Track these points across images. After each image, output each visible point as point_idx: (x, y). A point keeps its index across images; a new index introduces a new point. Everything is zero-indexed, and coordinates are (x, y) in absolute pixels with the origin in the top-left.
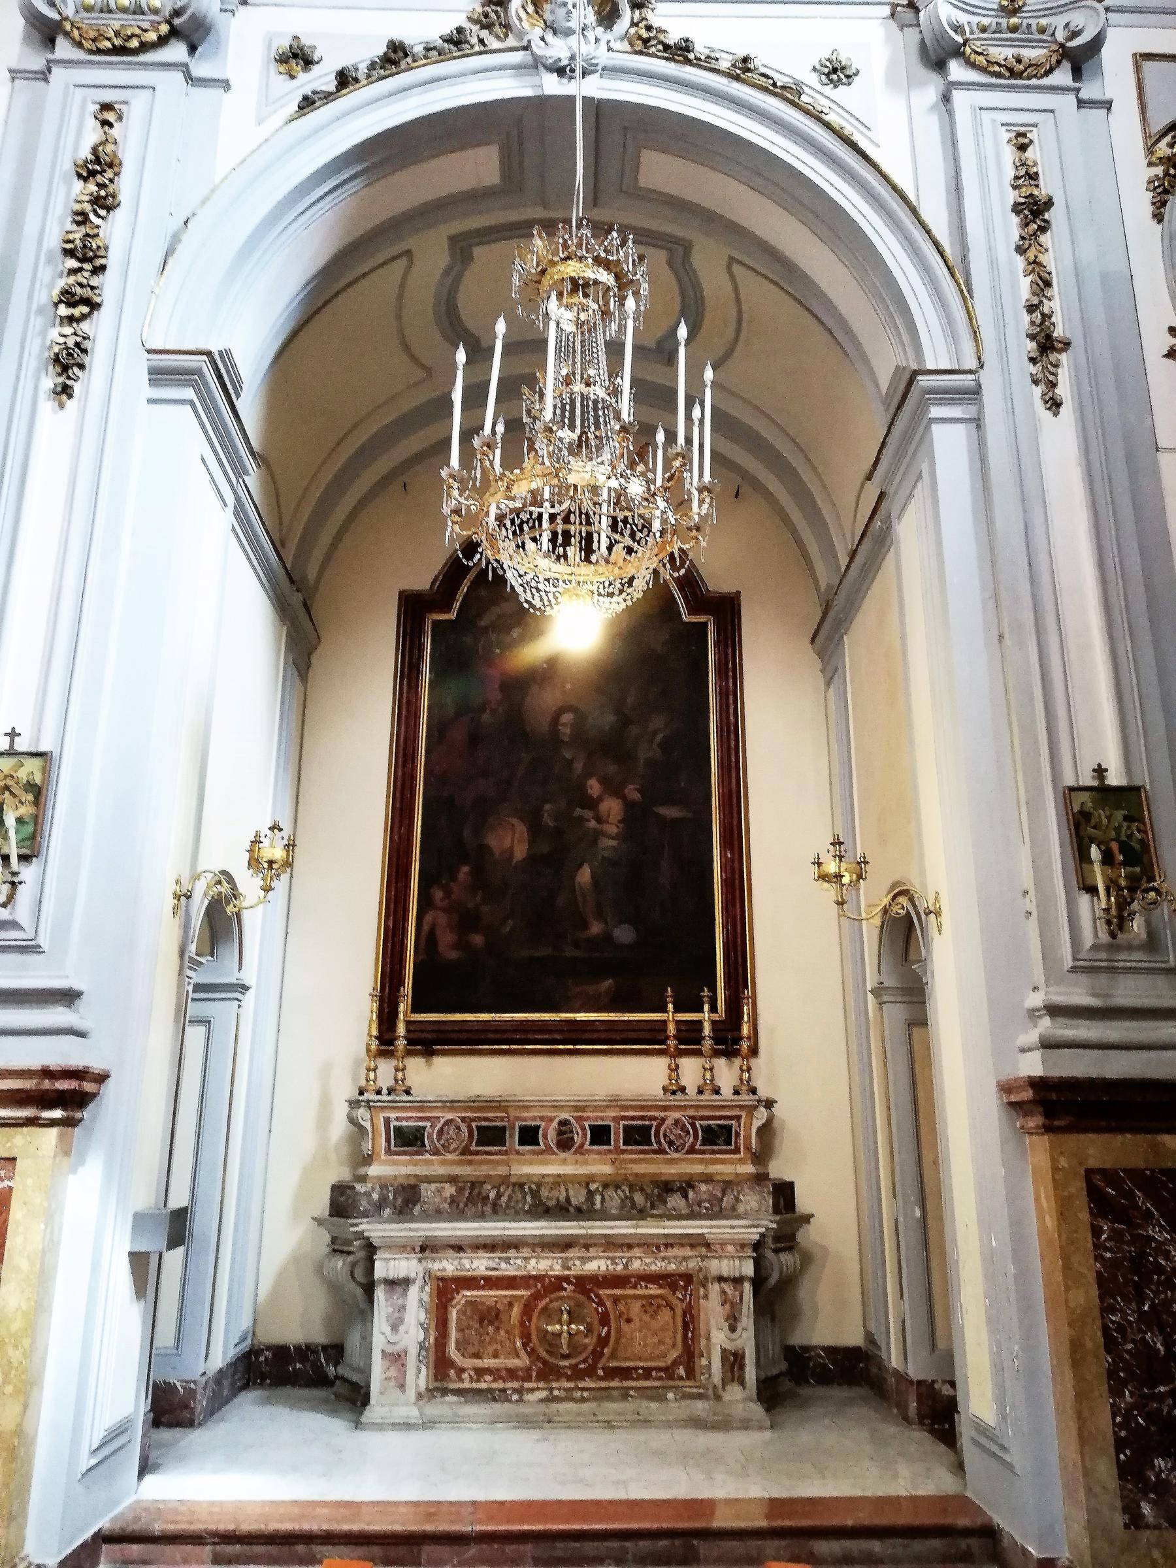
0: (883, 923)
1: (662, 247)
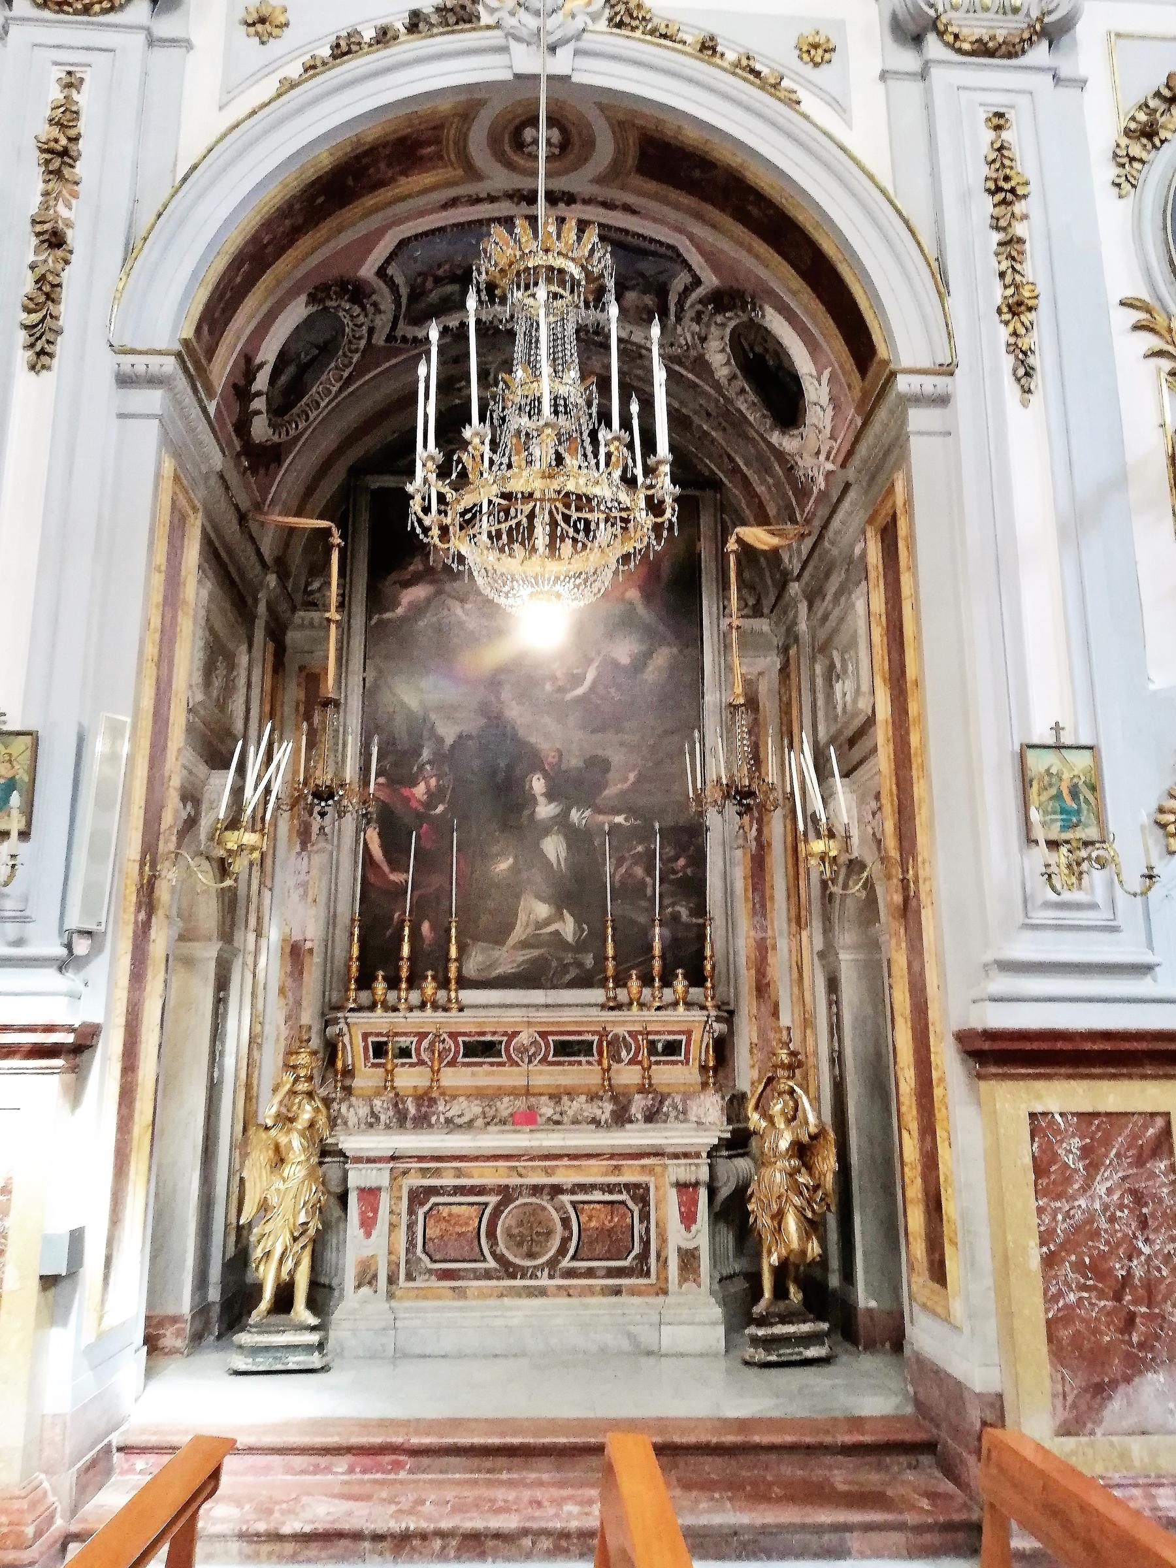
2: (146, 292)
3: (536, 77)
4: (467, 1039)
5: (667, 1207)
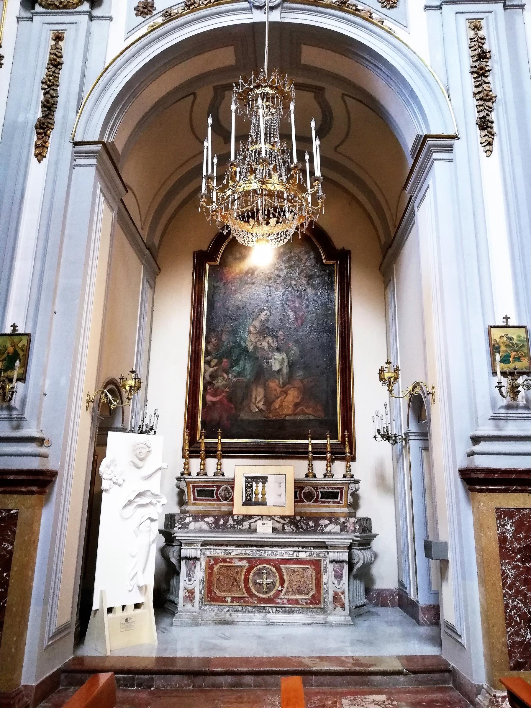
0: (410, 398)
1: (311, 91)
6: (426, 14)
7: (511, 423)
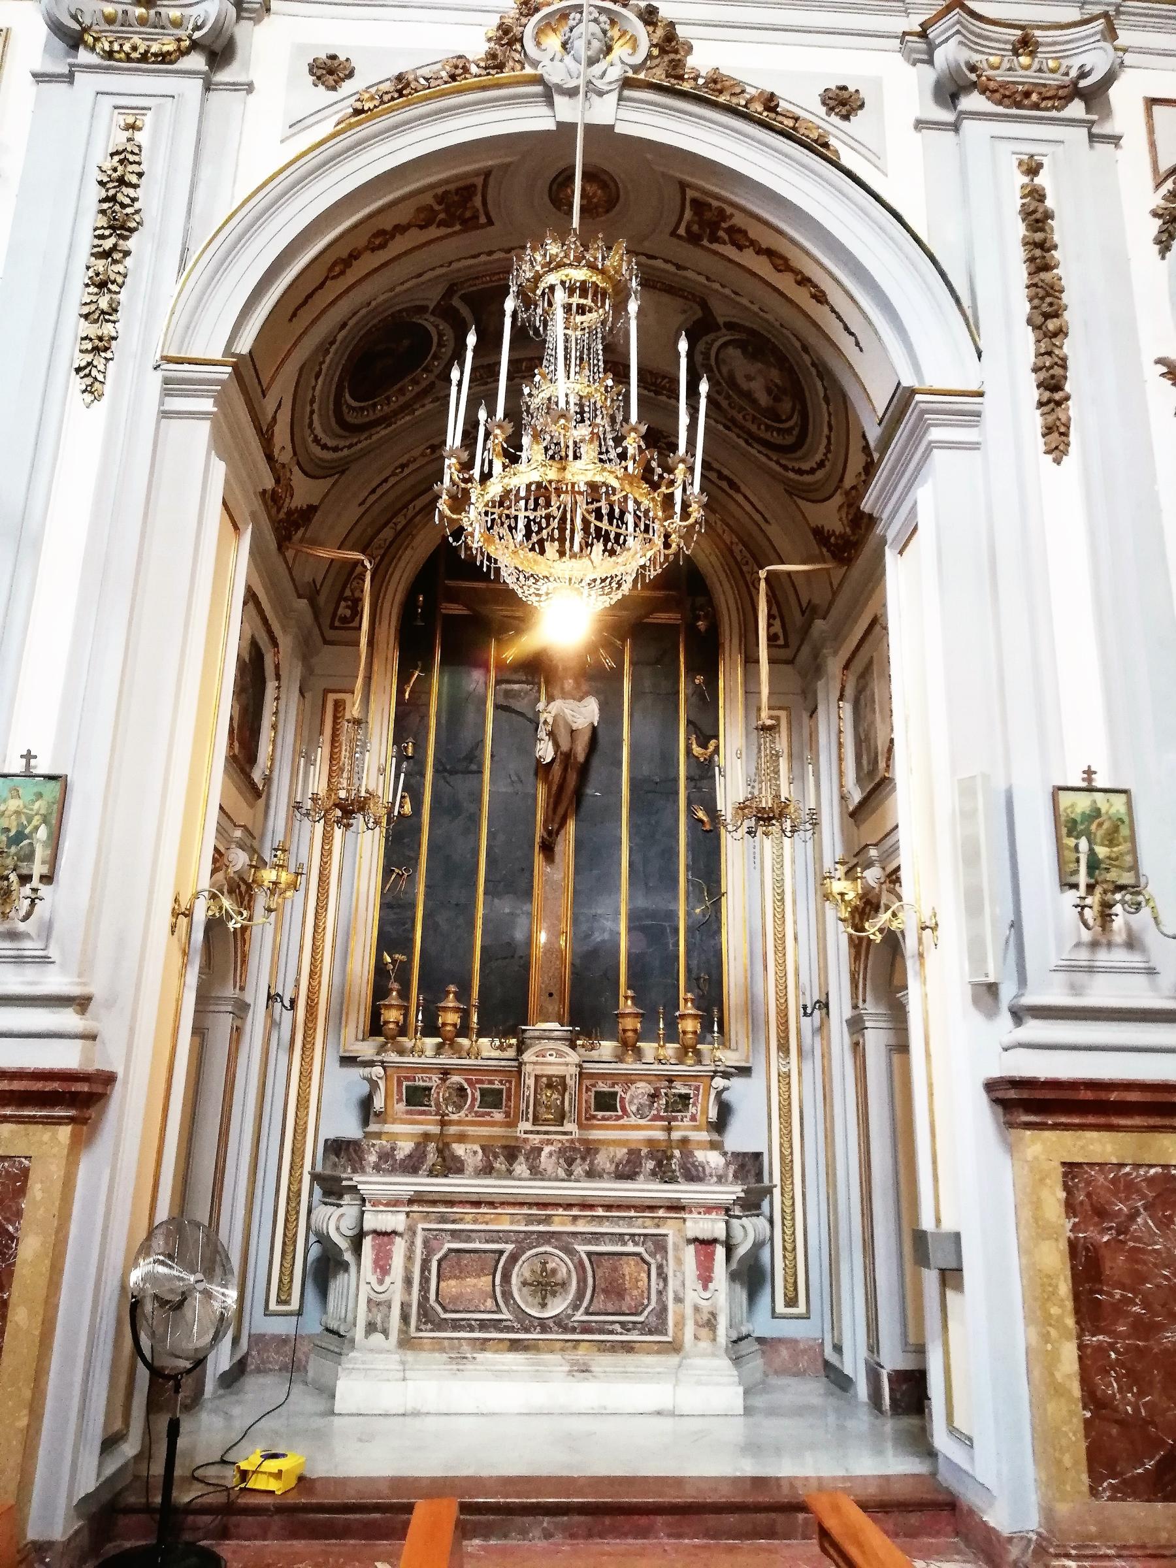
2: (203, 297)
3: (574, 126)
4: (477, 1103)
5: (661, 1051)
6: (918, 138)
7: (1100, 978)
